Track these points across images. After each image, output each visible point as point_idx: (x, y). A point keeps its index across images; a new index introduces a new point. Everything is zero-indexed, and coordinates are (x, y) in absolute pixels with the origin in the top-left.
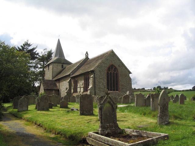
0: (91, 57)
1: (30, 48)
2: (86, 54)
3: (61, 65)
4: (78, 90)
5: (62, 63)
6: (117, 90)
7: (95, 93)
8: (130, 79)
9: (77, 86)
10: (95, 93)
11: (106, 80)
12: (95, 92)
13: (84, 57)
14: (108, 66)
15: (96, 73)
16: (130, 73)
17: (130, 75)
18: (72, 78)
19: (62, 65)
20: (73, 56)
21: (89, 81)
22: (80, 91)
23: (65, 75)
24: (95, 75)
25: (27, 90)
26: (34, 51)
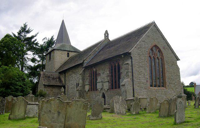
0: (112, 38)
1: (29, 35)
2: (105, 34)
3: (66, 53)
4: (99, 86)
5: (68, 51)
6: (163, 86)
7: (134, 91)
8: (178, 69)
9: (96, 80)
10: (134, 91)
11: (148, 69)
12: (133, 89)
13: (102, 38)
14: (150, 46)
15: (133, 58)
16: (178, 59)
17: (178, 62)
18: (86, 68)
19: (68, 54)
20: (83, 39)
21: (121, 71)
22: (102, 88)
23: (77, 64)
24: (133, 60)
25: (20, 86)
26: (33, 40)
